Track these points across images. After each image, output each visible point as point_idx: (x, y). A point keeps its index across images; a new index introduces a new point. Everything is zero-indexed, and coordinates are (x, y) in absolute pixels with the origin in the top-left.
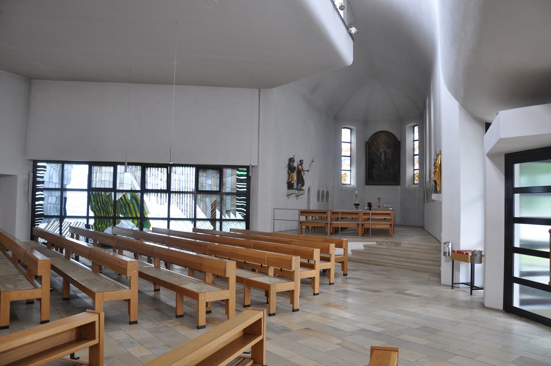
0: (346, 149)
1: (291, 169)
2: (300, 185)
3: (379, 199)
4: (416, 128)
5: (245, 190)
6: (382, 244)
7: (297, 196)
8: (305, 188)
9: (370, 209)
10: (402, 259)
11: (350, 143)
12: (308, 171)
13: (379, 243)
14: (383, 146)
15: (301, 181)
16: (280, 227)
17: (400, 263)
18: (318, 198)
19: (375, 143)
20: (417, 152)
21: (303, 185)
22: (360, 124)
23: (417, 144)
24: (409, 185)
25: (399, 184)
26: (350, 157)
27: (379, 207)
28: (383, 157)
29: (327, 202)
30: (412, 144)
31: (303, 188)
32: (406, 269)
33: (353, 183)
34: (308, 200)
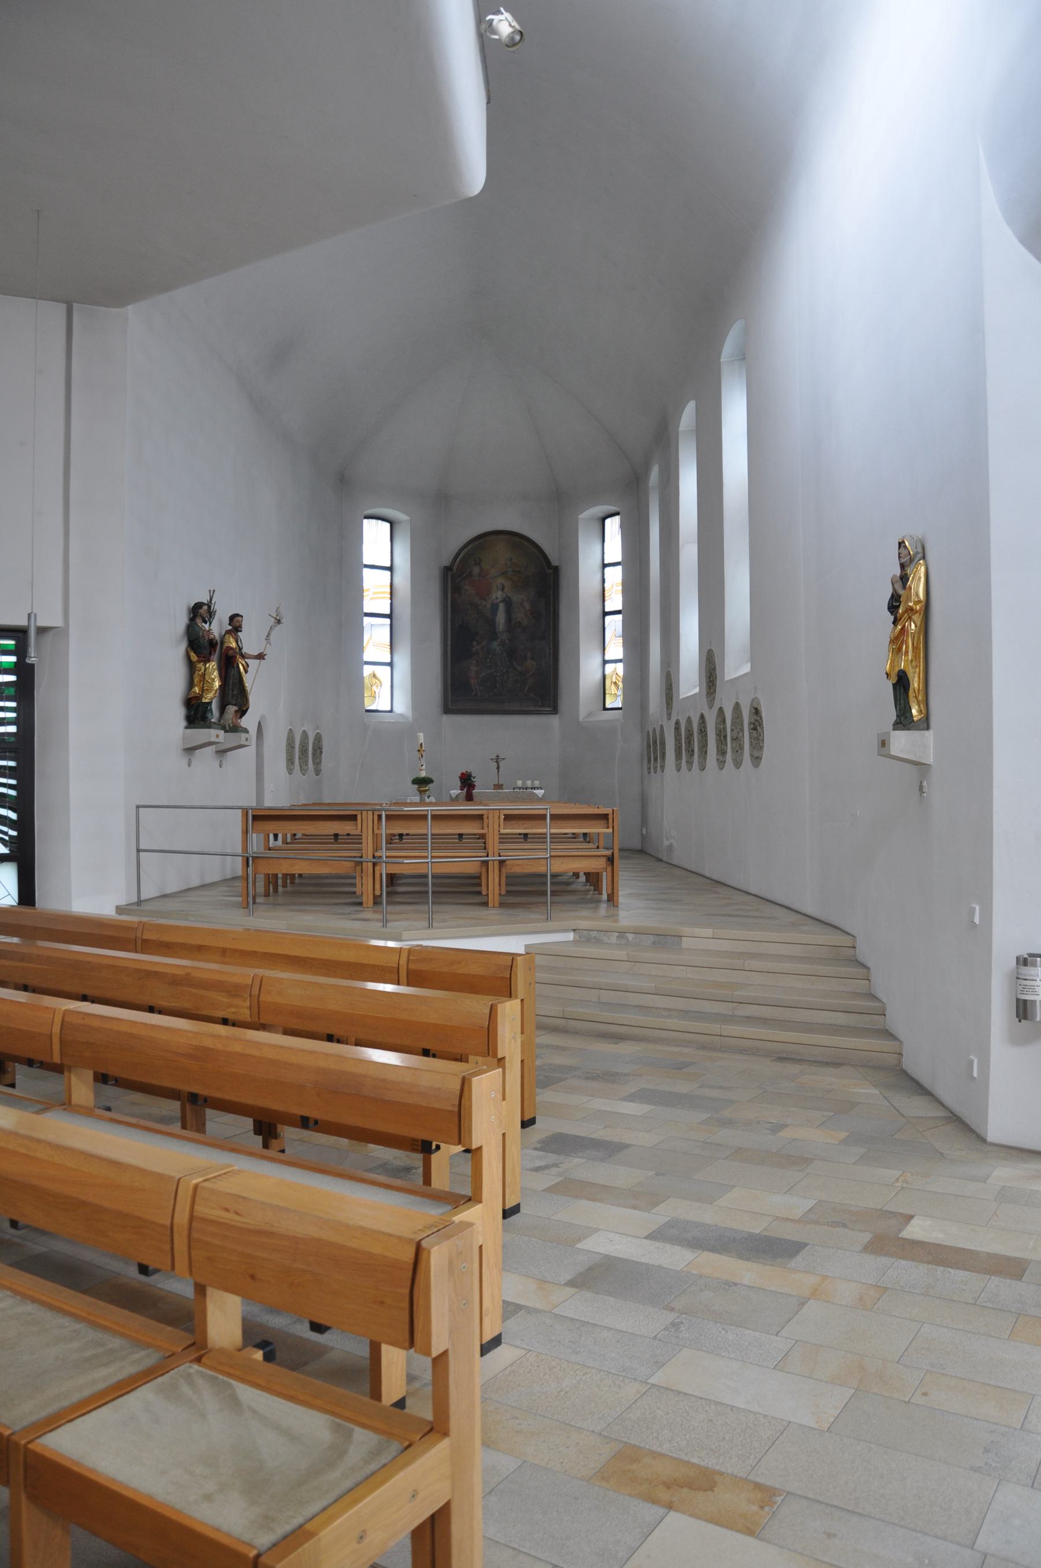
0: (375, 591)
1: (199, 645)
2: (232, 709)
3: (497, 760)
4: (613, 526)
5: (12, 729)
6: (598, 941)
7: (222, 753)
8: (248, 721)
9: (469, 798)
10: (311, 889)
11: (390, 569)
12: (261, 656)
13: (585, 938)
14: (500, 581)
15: (235, 694)
16: (163, 877)
17: (715, 1028)
18: (290, 761)
19: (476, 570)
20: (615, 601)
21: (242, 712)
22: (426, 505)
23: (614, 577)
24: (590, 714)
25: (555, 710)
26: (390, 616)
27: (498, 786)
28: (501, 618)
29: (318, 772)
30: (599, 576)
31: (244, 722)
32: (742, 1051)
33: (402, 706)
34: (256, 771)
